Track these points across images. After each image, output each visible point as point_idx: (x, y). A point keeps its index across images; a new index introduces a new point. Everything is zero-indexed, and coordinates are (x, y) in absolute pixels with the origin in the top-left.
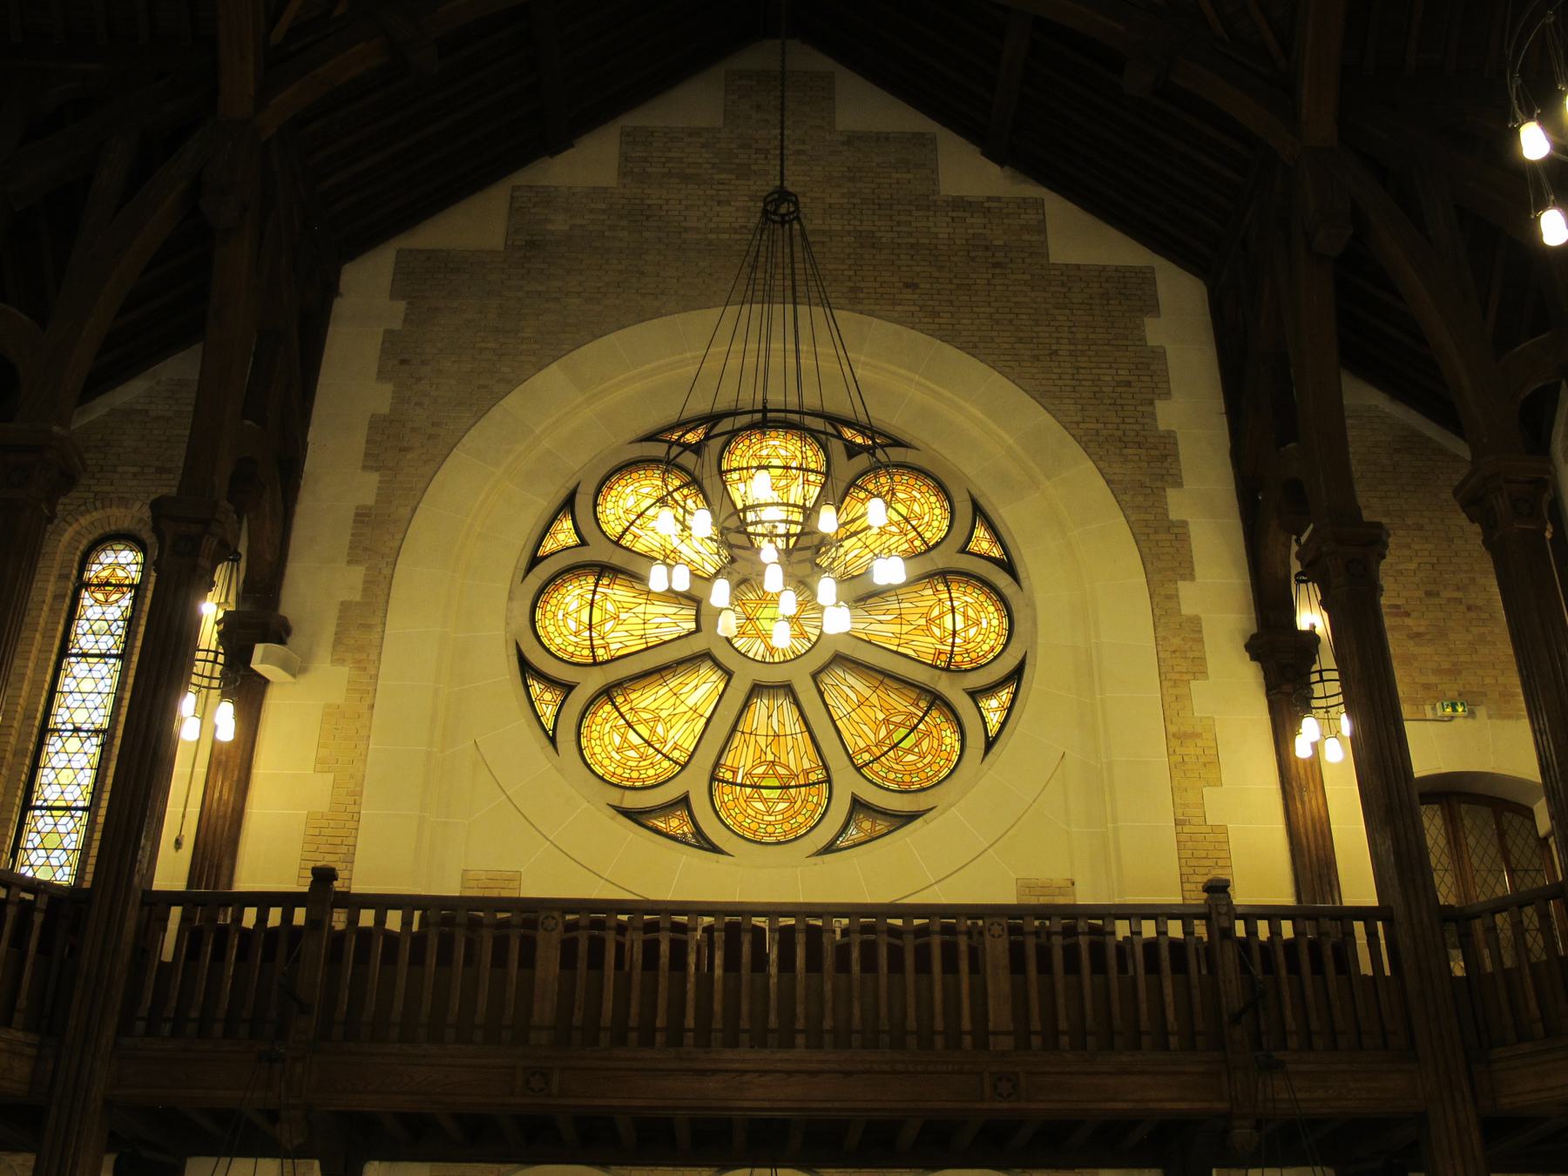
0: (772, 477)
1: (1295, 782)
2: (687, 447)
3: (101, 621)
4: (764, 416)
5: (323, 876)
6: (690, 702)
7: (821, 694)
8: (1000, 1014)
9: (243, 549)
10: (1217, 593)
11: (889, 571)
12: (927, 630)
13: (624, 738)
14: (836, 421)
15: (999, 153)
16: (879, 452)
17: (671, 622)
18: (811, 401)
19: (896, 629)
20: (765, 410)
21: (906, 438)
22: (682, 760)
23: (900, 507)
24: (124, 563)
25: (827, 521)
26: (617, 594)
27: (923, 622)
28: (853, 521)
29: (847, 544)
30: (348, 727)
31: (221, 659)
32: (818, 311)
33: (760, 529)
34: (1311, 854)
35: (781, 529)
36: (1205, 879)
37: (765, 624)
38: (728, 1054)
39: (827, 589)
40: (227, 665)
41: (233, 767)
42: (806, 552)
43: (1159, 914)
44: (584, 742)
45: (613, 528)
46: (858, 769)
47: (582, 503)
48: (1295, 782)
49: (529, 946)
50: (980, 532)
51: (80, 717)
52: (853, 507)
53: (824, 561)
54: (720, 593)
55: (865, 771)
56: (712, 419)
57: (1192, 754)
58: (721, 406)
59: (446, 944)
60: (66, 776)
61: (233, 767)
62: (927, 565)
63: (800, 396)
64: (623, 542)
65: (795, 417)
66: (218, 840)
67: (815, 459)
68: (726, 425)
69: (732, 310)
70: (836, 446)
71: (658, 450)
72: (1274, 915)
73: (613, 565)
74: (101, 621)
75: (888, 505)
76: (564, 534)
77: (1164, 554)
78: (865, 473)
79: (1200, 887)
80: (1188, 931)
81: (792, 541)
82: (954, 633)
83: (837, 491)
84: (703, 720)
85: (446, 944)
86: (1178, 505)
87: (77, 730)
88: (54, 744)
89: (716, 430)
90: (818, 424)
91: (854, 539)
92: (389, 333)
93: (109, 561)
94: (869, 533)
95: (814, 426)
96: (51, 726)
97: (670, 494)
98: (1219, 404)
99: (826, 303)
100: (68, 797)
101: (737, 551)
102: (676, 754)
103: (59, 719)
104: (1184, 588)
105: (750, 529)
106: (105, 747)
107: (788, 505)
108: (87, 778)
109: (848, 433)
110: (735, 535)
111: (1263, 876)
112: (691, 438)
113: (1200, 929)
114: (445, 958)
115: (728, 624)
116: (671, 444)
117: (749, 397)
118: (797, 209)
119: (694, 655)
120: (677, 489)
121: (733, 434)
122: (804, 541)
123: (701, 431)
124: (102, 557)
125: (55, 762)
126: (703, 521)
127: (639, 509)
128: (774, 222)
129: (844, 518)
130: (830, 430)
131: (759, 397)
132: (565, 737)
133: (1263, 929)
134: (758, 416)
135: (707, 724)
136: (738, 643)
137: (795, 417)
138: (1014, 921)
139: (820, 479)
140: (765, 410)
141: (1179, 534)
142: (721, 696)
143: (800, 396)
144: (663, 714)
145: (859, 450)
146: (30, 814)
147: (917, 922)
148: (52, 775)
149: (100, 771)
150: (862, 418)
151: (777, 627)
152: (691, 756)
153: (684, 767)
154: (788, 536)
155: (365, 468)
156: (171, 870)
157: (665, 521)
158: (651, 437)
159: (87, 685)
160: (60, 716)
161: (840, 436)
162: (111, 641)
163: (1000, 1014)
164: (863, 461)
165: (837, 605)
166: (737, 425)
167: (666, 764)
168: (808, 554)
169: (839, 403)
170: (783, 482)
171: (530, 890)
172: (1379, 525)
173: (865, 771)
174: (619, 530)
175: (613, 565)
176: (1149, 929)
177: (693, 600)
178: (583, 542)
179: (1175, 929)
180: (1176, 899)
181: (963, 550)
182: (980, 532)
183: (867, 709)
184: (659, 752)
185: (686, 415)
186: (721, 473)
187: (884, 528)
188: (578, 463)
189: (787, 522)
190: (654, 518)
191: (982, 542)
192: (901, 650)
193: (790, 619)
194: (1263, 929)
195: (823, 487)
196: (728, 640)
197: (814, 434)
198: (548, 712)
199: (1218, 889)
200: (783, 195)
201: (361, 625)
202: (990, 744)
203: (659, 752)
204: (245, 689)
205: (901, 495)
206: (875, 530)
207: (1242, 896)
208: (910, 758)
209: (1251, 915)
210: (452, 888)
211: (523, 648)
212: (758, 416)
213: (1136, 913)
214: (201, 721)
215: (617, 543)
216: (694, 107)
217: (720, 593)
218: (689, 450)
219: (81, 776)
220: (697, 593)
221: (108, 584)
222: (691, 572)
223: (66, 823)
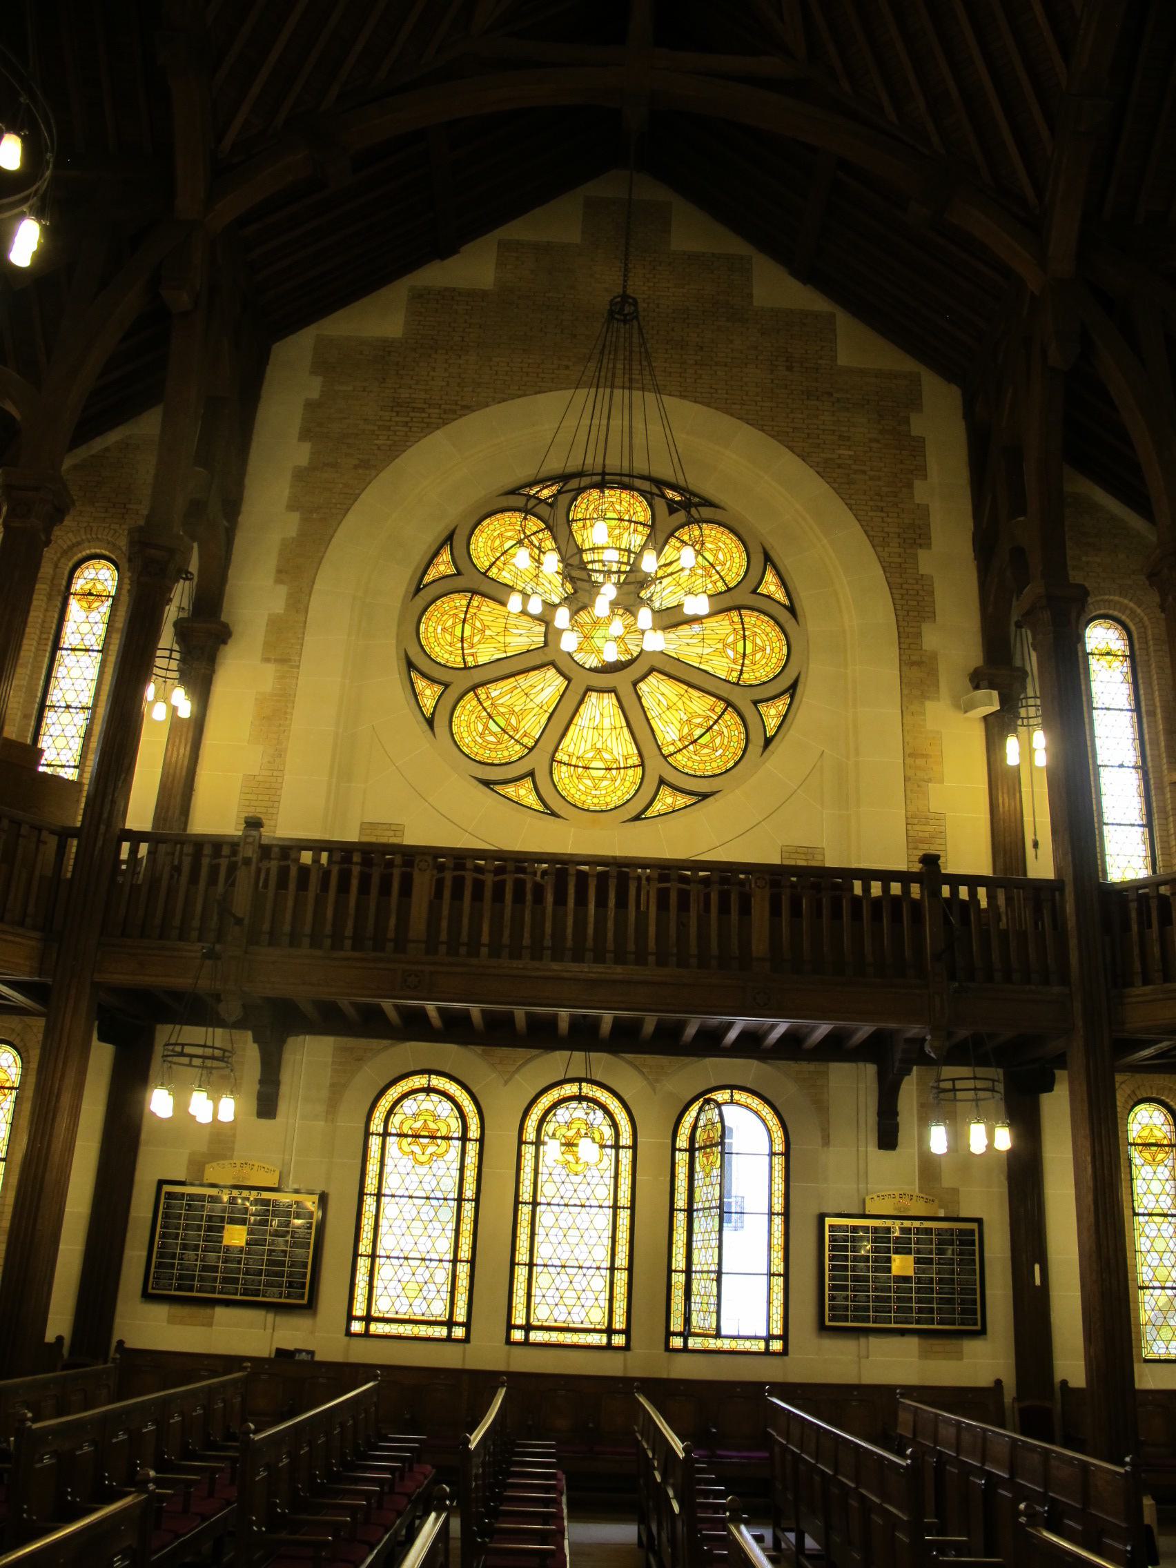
0: (609, 527)
1: (1001, 782)
2: (544, 501)
3: (86, 624)
4: (603, 479)
5: (254, 824)
6: (538, 701)
7: (639, 698)
8: (759, 945)
9: (194, 567)
10: (955, 638)
11: (698, 605)
12: (722, 653)
13: (486, 727)
14: (661, 484)
15: (808, 274)
16: (693, 511)
17: (527, 637)
18: (640, 466)
19: (699, 650)
20: (604, 474)
21: (716, 501)
22: (530, 745)
23: (707, 555)
24: (100, 577)
25: (649, 563)
26: (486, 610)
27: (720, 646)
28: (671, 563)
29: (665, 581)
30: (275, 715)
31: (176, 655)
32: (650, 397)
33: (597, 566)
34: (1007, 840)
35: (615, 568)
36: (921, 853)
37: (598, 642)
38: (555, 966)
39: (645, 617)
40: (182, 660)
41: (193, 732)
42: (634, 587)
43: (886, 877)
44: (455, 729)
45: (482, 562)
46: (665, 757)
47: (459, 540)
48: (1001, 782)
49: (407, 881)
50: (770, 577)
51: (71, 698)
52: (669, 552)
53: (644, 594)
54: (562, 617)
55: (669, 759)
56: (564, 478)
57: (917, 763)
58: (569, 470)
59: (345, 877)
60: (61, 742)
61: (193, 732)
62: (727, 601)
63: (631, 461)
64: (490, 574)
65: (626, 479)
66: (178, 791)
67: (641, 511)
68: (573, 484)
69: (582, 393)
70: (660, 504)
71: (519, 501)
72: (973, 882)
73: (484, 587)
74: (86, 624)
75: (698, 553)
76: (444, 565)
77: (912, 605)
78: (682, 526)
79: (917, 858)
80: (906, 890)
81: (623, 577)
82: (744, 655)
83: (658, 537)
84: (547, 715)
85: (345, 877)
86: (926, 562)
87: (68, 707)
88: (50, 717)
89: (567, 488)
90: (646, 485)
91: (670, 579)
92: (310, 406)
93: (91, 576)
94: (682, 574)
95: (643, 488)
96: (48, 703)
97: (527, 537)
98: (977, 605)
99: (658, 390)
100: (87, 643)
101: (579, 584)
102: (525, 740)
103: (54, 698)
104: (922, 554)
105: (590, 566)
106: (113, 608)
107: (620, 549)
108: (77, 744)
109: (670, 494)
110: (579, 578)
111: (969, 854)
112: (546, 493)
113: (915, 890)
114: (344, 887)
115: (569, 642)
116: (529, 497)
117: (593, 461)
118: (636, 311)
119: (544, 657)
120: (534, 534)
121: (580, 490)
122: (632, 578)
123: (555, 488)
124: (86, 573)
125: (52, 730)
126: (552, 562)
127: (502, 544)
128: (618, 320)
129: (662, 563)
130: (655, 490)
131: (600, 460)
132: (440, 723)
133: (964, 892)
134: (598, 478)
135: (550, 718)
136: (577, 657)
137: (626, 479)
138: (774, 877)
139: (647, 531)
140: (604, 474)
141: (916, 448)
142: (562, 696)
143: (631, 461)
144: (517, 709)
145: (679, 506)
146: (59, 653)
147: (701, 874)
148: (50, 740)
149: (110, 625)
150: (682, 483)
151: (605, 636)
152: (537, 742)
153: (531, 750)
154: (619, 572)
155: (312, 373)
156: (140, 810)
157: (522, 558)
158: (513, 492)
159: (61, 742)
160: (55, 697)
161: (663, 496)
162: (69, 756)
163: (759, 945)
164: (681, 516)
165: (653, 629)
166: (582, 485)
167: (518, 747)
168: (632, 588)
169: (663, 470)
170: (617, 531)
171: (410, 839)
172: (1082, 587)
173: (669, 759)
174: (487, 564)
175: (484, 587)
176: (876, 889)
177: (545, 619)
178: (447, 686)
179: (896, 888)
180: (903, 867)
181: (754, 592)
182: (770, 577)
183: (674, 712)
184: (512, 737)
185: (540, 476)
186: (568, 521)
187: (696, 567)
188: (453, 514)
189: (619, 562)
190: (515, 554)
191: (771, 585)
192: (702, 667)
193: (616, 639)
194: (964, 892)
195: (649, 536)
196: (570, 654)
197: (643, 493)
198: (428, 703)
199: (931, 861)
200: (625, 297)
201: (284, 646)
202: (768, 742)
203: (512, 737)
204: (199, 672)
205: (708, 545)
206: (687, 572)
207: (951, 866)
208: (706, 751)
209: (956, 880)
210: (352, 836)
211: (410, 654)
212: (598, 478)
213: (867, 876)
214: (165, 703)
215: (484, 574)
216: (558, 224)
217: (562, 617)
218: (547, 500)
219: (95, 628)
220: (547, 618)
221: (90, 594)
222: (544, 602)
223: (85, 658)
